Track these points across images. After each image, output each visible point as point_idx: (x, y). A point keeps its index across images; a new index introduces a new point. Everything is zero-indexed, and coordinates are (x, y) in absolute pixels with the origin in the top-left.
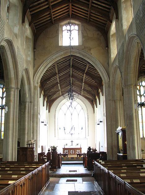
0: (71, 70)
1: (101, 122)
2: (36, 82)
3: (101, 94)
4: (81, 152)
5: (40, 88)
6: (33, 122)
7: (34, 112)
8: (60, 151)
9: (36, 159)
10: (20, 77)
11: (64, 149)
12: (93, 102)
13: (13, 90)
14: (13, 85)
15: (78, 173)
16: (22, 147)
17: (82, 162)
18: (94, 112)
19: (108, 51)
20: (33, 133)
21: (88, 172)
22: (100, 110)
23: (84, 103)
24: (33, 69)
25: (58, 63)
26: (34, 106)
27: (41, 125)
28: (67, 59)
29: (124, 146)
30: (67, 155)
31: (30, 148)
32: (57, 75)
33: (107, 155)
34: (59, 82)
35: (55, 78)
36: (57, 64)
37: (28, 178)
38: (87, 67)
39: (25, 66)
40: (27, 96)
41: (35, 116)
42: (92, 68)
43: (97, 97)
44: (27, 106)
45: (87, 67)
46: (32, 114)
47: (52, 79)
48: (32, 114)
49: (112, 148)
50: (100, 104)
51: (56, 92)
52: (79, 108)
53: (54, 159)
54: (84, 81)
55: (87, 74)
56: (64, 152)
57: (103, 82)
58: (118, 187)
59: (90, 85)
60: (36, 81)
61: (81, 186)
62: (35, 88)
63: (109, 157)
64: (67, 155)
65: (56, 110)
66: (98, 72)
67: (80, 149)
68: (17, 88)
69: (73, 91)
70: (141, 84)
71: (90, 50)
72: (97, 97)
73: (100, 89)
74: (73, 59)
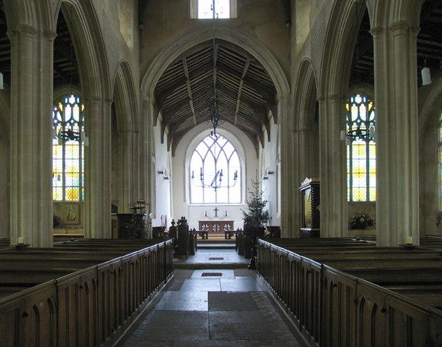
0: (215, 73)
1: (269, 173)
2: (145, 94)
3: (272, 121)
4: (232, 228)
5: (154, 106)
6: (142, 169)
7: (142, 153)
8: (193, 225)
9: (150, 235)
10: (112, 77)
11: (201, 223)
12: (254, 135)
13: (100, 103)
14: (98, 93)
15: (226, 261)
16: (122, 213)
17: (235, 245)
18: (258, 158)
19: (290, 32)
20: (142, 190)
21: (244, 261)
22: (270, 154)
23: (239, 140)
24: (140, 67)
25: (189, 55)
26: (142, 140)
27: (159, 178)
28: (207, 46)
29: (316, 213)
30: (207, 233)
31: (138, 215)
32: (188, 82)
33: (281, 232)
34: (190, 97)
35: (181, 89)
36: (187, 58)
37: (129, 262)
38: (247, 66)
39: (121, 57)
40: (129, 119)
41: (144, 162)
42: (257, 67)
43: (264, 128)
44: (129, 138)
45: (247, 66)
46: (139, 154)
47: (178, 90)
48: (139, 154)
49: (290, 220)
50: (269, 141)
51: (188, 116)
52: (229, 148)
53: (183, 240)
54: (239, 96)
55: (249, 80)
56: (200, 228)
57: (279, 95)
58: (307, 277)
59: (253, 105)
60: (146, 90)
61: (230, 283)
62: (144, 104)
63: (285, 234)
64: (207, 233)
65: (186, 153)
66: (270, 78)
67: (231, 223)
68: (107, 100)
69: (219, 117)
70: (352, 101)
71: (253, 28)
72: (264, 128)
73: (270, 112)
74: (219, 50)
